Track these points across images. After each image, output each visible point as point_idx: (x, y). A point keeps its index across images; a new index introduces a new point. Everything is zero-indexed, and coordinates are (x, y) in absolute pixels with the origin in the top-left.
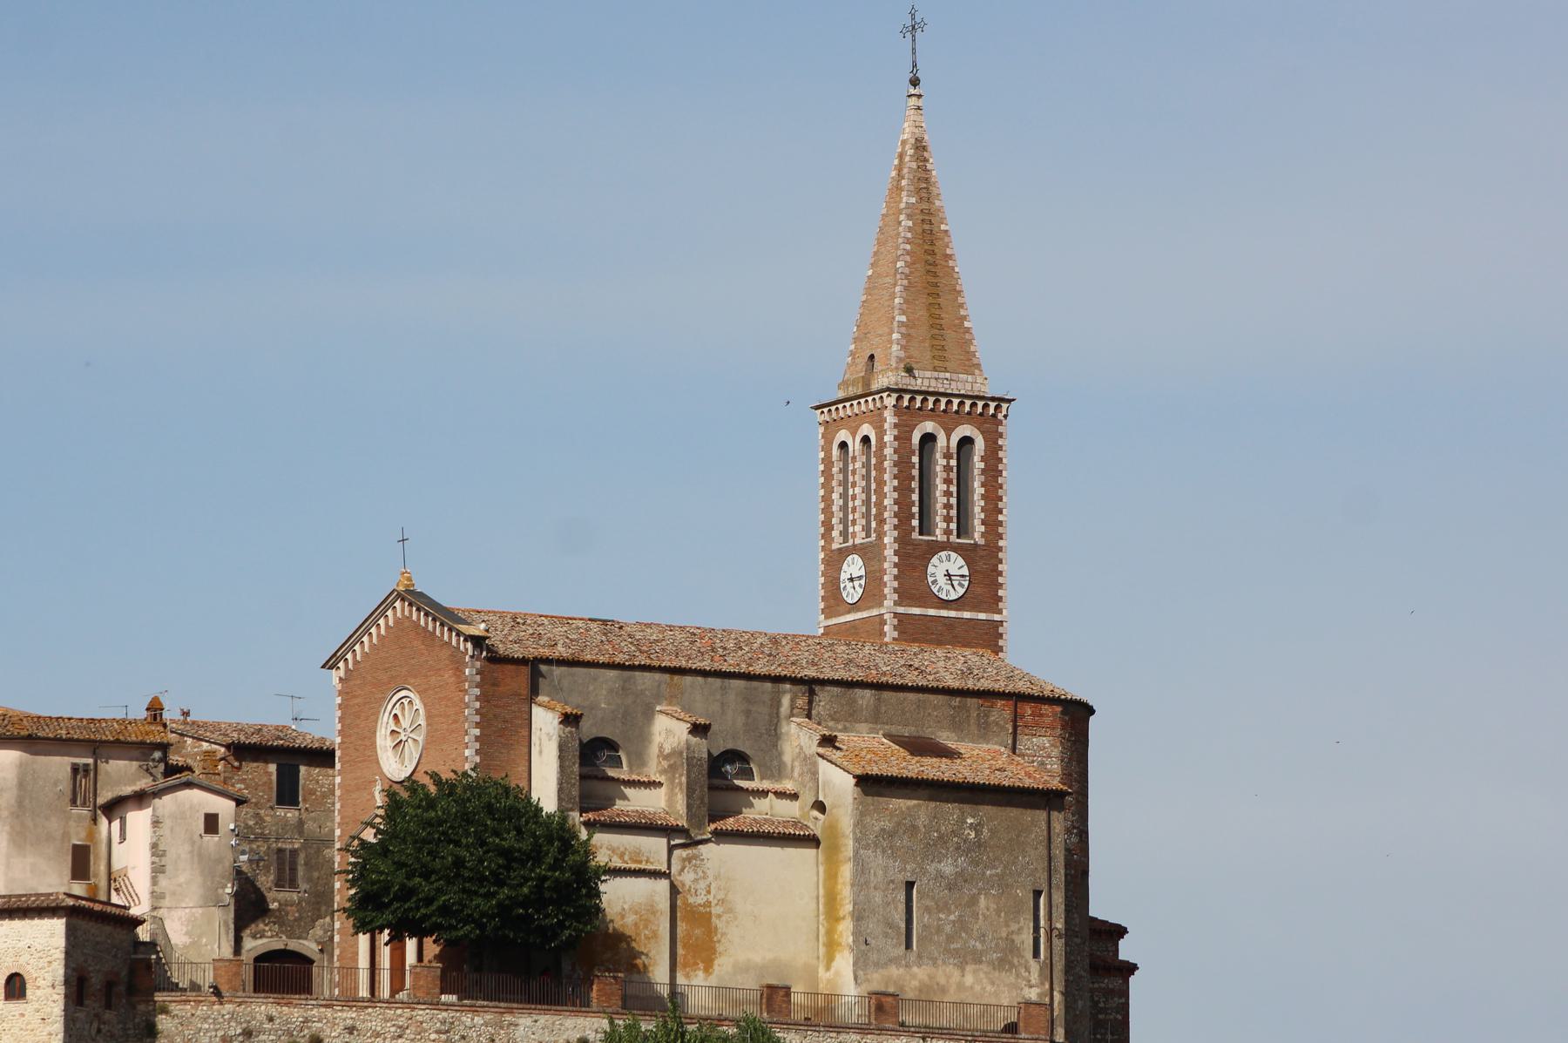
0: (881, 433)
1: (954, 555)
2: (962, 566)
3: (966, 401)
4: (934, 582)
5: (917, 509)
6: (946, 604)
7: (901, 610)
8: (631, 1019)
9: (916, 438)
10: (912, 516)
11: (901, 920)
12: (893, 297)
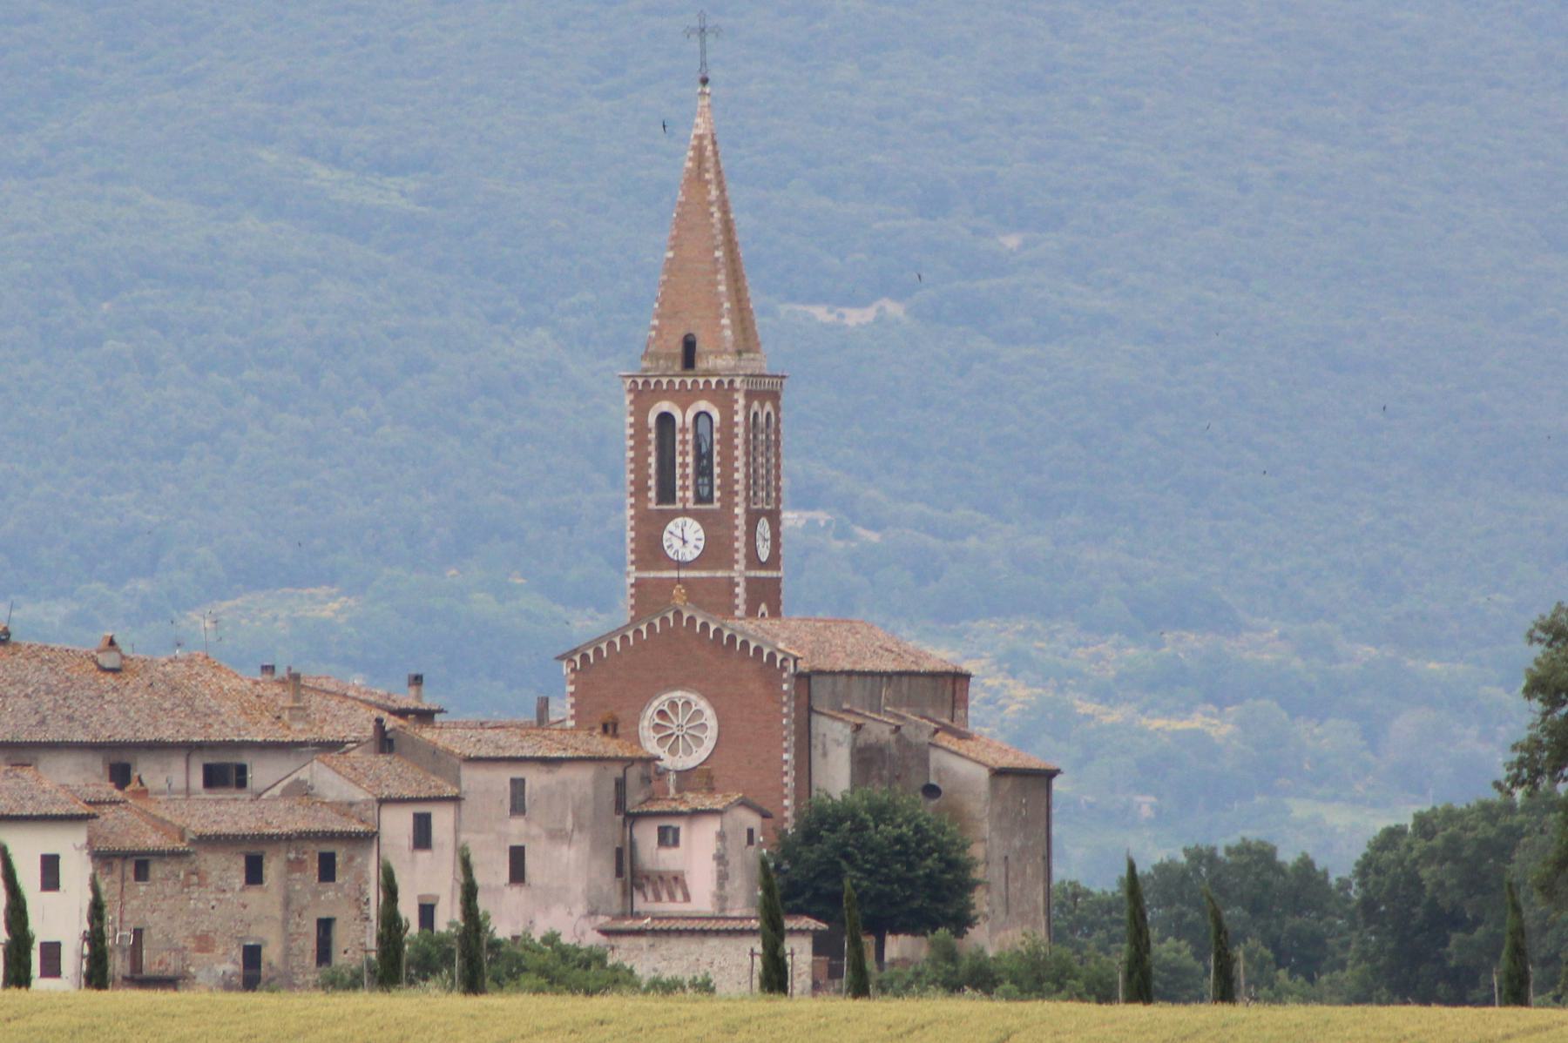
0: (727, 414)
1: (689, 521)
2: (698, 531)
3: (661, 379)
4: (670, 546)
5: (677, 483)
6: (680, 565)
7: (752, 574)
8: (1119, 945)
9: (652, 419)
10: (719, 488)
11: (68, 810)
12: (715, 284)
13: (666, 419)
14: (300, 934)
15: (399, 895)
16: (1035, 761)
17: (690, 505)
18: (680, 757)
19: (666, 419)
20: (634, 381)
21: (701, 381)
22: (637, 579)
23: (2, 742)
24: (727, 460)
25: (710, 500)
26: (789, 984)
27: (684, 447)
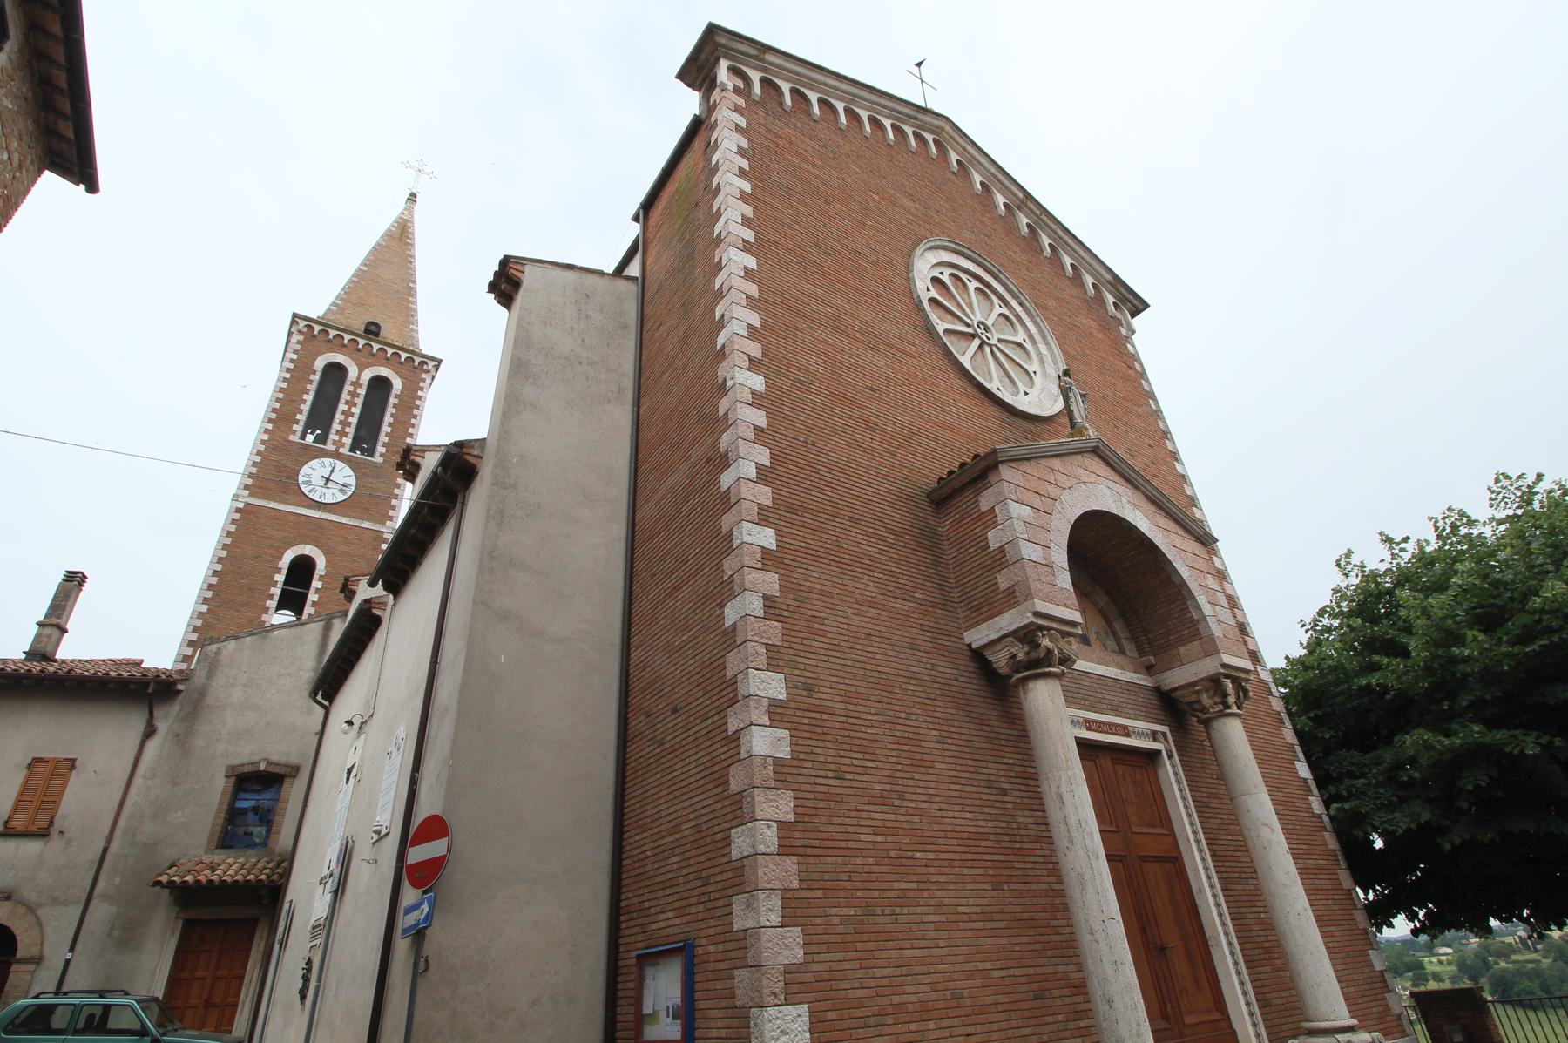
1: (340, 465)
9: (320, 364)
13: (335, 374)
14: (1399, 556)
15: (690, 89)
16: (72, 757)
17: (345, 450)
18: (1026, 394)
19: (335, 374)
20: (308, 326)
21: (376, 347)
22: (383, 524)
23: (1546, 917)
24: (900, 113)
25: (371, 452)
26: (1427, 1033)
27: (347, 417)
